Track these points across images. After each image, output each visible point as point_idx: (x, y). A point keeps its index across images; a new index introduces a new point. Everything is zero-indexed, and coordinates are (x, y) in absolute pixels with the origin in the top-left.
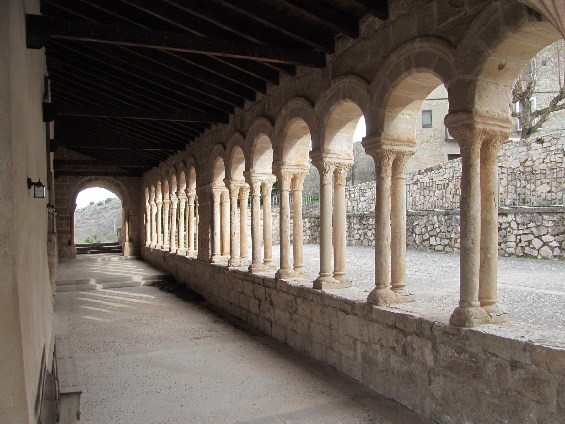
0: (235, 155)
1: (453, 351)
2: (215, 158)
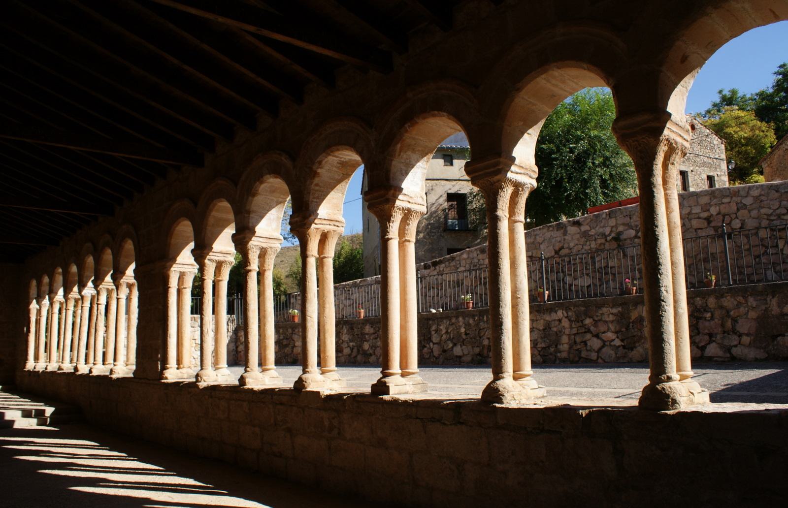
0: (214, 213)
2: (175, 220)
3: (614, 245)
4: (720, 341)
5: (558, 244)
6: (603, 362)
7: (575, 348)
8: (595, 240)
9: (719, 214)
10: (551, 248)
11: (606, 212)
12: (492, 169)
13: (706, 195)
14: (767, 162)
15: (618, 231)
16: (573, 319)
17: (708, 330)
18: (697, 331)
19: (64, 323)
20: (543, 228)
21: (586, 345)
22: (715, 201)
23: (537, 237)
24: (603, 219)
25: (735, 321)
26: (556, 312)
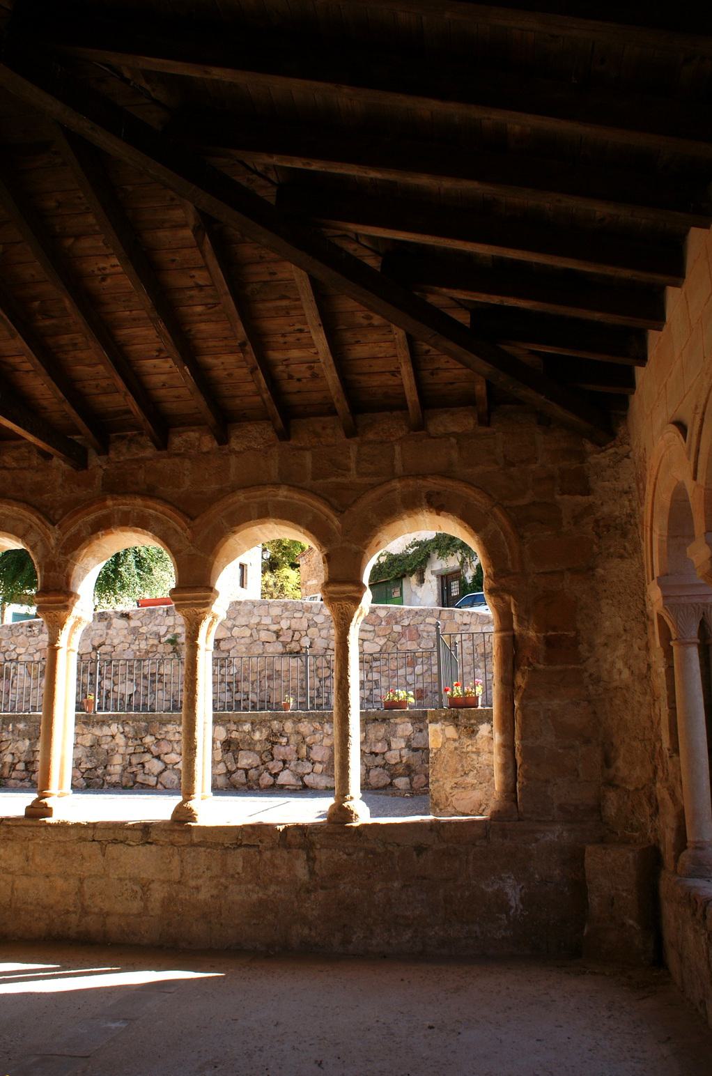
1: (341, 853)
3: (170, 648)
4: (293, 768)
5: (97, 639)
6: (163, 788)
7: (130, 770)
8: (146, 639)
9: (289, 628)
10: (89, 641)
11: (164, 608)
12: (201, 601)
13: (278, 606)
14: (305, 559)
15: (175, 632)
16: (130, 735)
17: (283, 756)
18: (271, 757)
21: (144, 767)
24: (159, 615)
25: (310, 747)
26: (109, 726)
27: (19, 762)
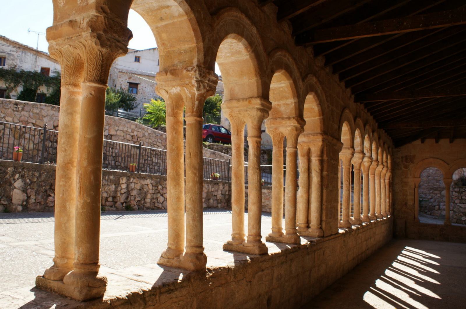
10: (52, 122)
19: (376, 190)
20: (48, 106)
22: (136, 129)
23: (42, 111)
26: (147, 180)
27: (109, 197)
